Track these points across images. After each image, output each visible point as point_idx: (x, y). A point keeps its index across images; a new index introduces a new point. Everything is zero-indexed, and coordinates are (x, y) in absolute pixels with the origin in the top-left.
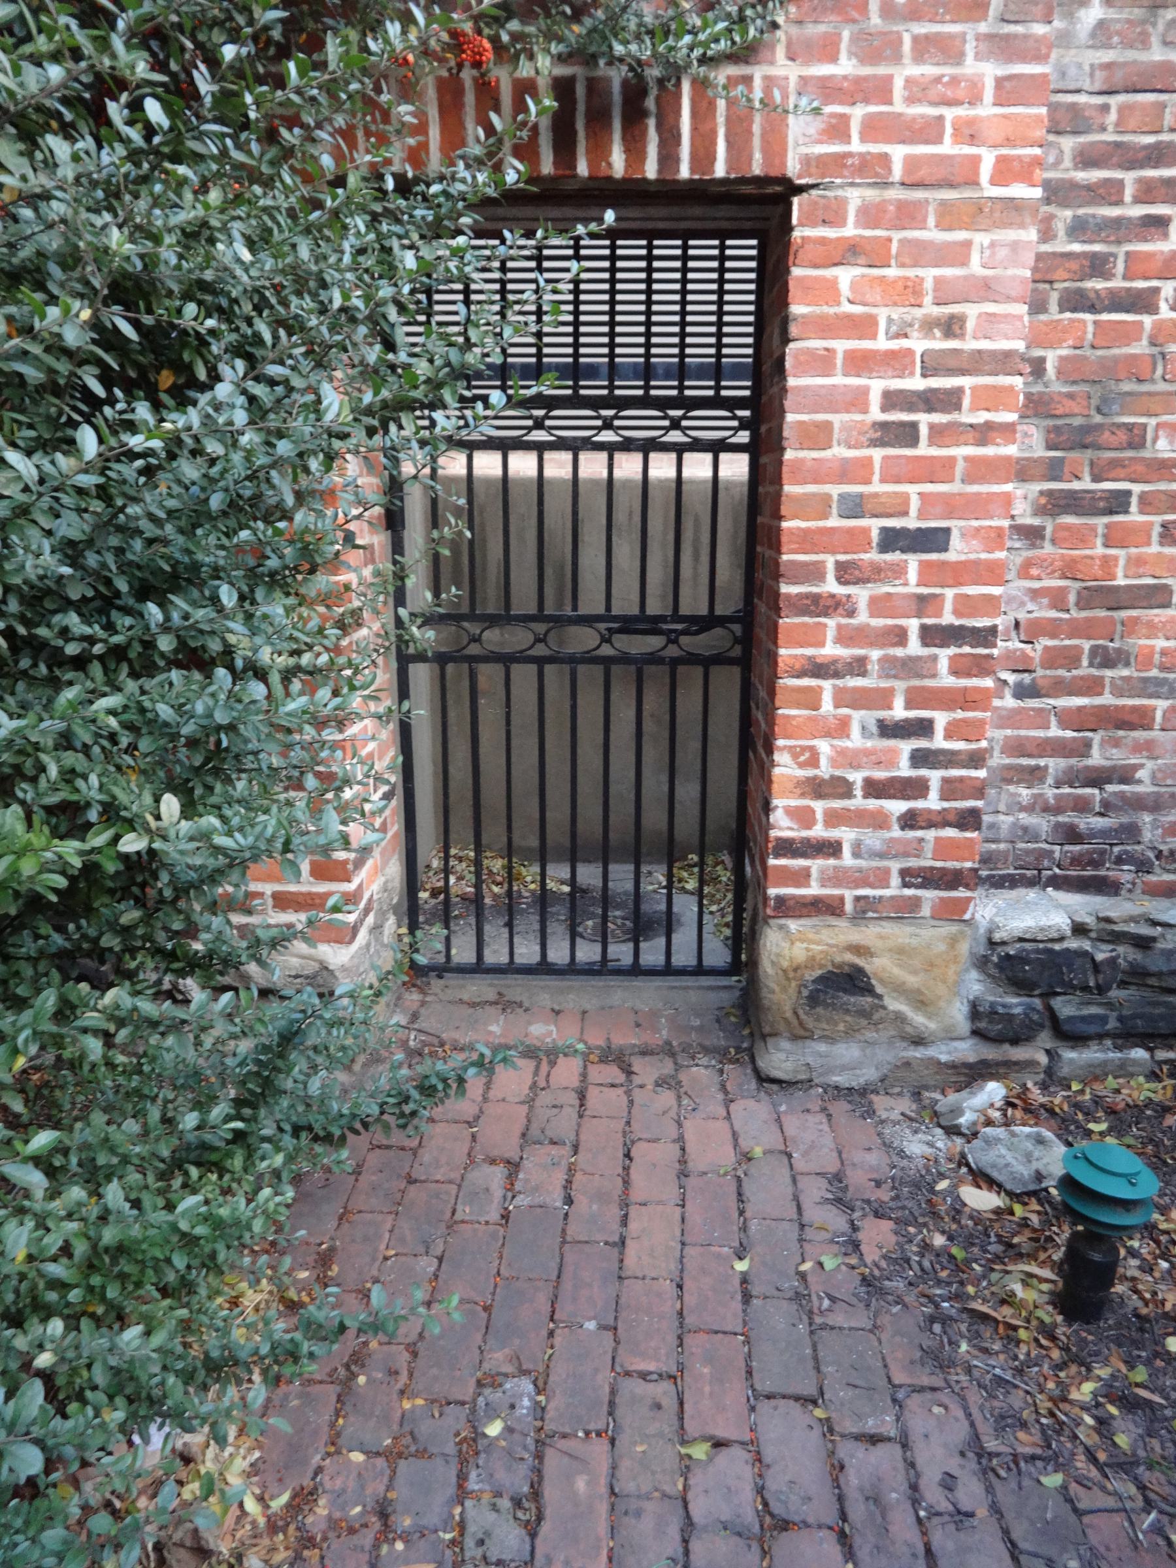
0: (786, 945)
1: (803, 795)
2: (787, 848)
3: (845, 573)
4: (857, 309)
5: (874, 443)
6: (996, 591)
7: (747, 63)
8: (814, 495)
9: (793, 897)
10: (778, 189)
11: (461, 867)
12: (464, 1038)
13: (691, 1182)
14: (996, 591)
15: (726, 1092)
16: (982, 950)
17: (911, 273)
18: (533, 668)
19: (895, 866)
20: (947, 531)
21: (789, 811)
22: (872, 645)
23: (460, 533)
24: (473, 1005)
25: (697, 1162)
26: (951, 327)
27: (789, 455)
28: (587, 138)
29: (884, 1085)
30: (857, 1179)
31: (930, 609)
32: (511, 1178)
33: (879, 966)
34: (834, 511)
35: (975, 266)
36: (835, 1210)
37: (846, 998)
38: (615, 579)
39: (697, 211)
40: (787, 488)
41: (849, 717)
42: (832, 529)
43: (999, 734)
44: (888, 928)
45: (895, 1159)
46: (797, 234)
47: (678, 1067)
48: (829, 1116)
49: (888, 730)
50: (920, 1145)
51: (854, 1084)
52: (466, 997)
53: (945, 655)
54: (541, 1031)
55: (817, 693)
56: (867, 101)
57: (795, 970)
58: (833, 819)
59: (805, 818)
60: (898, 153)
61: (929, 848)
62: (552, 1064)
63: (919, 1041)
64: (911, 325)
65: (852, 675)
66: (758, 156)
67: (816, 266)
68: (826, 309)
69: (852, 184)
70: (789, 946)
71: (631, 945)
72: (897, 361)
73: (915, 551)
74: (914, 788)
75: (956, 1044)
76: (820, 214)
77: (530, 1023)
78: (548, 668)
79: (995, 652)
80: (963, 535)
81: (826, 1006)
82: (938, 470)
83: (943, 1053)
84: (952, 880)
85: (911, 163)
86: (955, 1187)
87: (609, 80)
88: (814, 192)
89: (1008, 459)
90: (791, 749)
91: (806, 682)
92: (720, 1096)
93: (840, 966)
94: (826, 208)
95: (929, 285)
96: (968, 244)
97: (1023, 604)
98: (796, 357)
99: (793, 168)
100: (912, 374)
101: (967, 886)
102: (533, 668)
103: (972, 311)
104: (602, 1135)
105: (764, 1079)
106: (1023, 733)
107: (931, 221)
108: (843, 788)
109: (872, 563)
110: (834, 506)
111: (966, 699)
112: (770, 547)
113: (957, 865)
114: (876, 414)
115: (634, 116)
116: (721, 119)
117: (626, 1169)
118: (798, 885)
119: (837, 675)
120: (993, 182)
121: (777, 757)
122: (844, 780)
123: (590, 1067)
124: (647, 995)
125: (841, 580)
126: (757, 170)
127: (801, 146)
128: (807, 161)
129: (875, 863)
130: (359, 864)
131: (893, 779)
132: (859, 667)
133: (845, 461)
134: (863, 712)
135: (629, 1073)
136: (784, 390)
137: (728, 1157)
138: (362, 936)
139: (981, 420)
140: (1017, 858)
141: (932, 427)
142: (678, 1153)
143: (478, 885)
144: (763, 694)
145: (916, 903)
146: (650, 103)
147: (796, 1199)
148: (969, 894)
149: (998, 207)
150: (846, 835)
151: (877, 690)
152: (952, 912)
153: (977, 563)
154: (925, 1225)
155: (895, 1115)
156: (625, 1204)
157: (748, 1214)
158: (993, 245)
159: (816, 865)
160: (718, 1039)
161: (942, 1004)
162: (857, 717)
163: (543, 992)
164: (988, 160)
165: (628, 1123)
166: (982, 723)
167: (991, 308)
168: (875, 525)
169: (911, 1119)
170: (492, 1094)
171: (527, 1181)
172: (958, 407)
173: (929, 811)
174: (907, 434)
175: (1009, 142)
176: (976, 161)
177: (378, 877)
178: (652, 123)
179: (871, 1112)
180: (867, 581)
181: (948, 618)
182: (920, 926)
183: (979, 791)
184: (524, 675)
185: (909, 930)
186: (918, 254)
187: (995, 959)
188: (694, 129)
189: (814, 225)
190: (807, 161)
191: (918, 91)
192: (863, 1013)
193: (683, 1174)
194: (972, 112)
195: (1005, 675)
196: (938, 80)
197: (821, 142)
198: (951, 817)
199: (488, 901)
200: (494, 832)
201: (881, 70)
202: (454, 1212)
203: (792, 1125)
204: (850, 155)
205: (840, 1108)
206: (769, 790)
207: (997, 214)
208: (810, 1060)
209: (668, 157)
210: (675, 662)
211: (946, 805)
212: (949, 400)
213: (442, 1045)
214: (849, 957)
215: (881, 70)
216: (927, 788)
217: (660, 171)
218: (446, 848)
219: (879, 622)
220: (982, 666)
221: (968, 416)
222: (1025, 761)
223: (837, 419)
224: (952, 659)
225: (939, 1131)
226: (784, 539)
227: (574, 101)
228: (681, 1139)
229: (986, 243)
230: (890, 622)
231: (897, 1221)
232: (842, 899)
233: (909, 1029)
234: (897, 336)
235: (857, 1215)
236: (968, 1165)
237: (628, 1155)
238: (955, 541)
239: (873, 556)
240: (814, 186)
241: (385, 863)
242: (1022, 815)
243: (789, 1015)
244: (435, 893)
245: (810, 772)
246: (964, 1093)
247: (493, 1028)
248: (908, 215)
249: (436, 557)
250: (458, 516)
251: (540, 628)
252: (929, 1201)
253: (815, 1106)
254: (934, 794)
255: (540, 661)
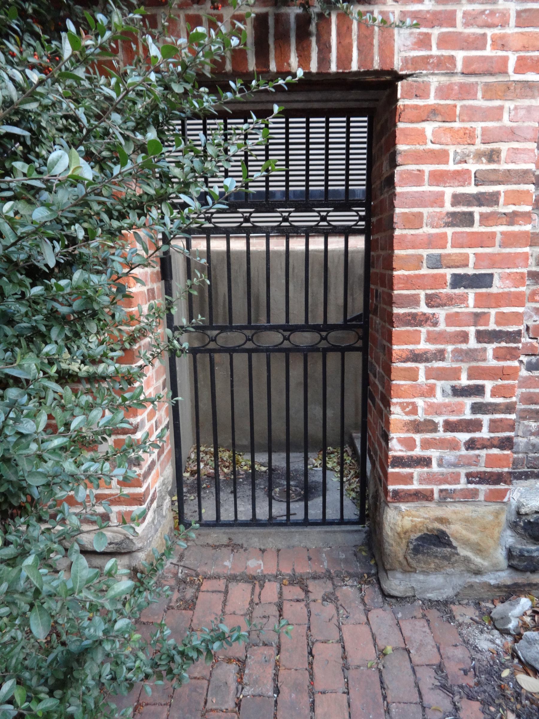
0: (399, 518)
1: (408, 431)
2: (399, 462)
3: (431, 301)
4: (437, 147)
5: (447, 225)
6: (520, 310)
7: (370, 4)
8: (413, 255)
9: (403, 490)
10: (388, 78)
11: (206, 458)
12: (212, 570)
13: (351, 674)
14: (520, 310)
15: (365, 604)
16: (513, 518)
17: (468, 125)
18: (246, 355)
19: (463, 471)
20: (491, 275)
21: (400, 440)
22: (448, 342)
23: (203, 282)
24: (215, 547)
25: (354, 659)
26: (492, 156)
27: (397, 232)
28: (276, 49)
29: (457, 599)
30: (453, 668)
31: (482, 321)
32: (241, 672)
33: (454, 530)
34: (425, 265)
35: (506, 121)
36: (443, 695)
37: (435, 549)
38: (286, 304)
39: (338, 95)
40: (397, 252)
41: (435, 385)
42: (424, 275)
43: (519, 391)
44: (459, 507)
45: (473, 653)
46: (400, 103)
47: (335, 586)
48: (428, 621)
49: (458, 392)
50: (487, 642)
51: (440, 598)
52: (210, 542)
53: (490, 348)
54: (255, 565)
55: (416, 371)
56: (441, 25)
57: (405, 533)
58: (426, 444)
59: (409, 444)
60: (460, 55)
61: (483, 461)
62: (262, 587)
63: (478, 572)
64: (468, 156)
65: (436, 360)
66: (377, 58)
67: (412, 122)
68: (418, 147)
69: (433, 74)
70: (401, 520)
71: (302, 504)
72: (460, 177)
73: (472, 287)
74: (473, 426)
75: (500, 573)
76: (414, 92)
77: (248, 559)
78: (254, 355)
79: (520, 345)
80: (500, 278)
81: (424, 554)
82: (485, 240)
83: (492, 579)
84: (498, 479)
85: (467, 61)
86: (513, 674)
87: (288, 15)
88: (410, 79)
89: (526, 233)
90: (401, 404)
91: (409, 365)
92: (361, 607)
93: (431, 530)
94: (418, 88)
95: (479, 132)
96: (501, 108)
97: (531, 316)
98: (401, 175)
99: (397, 65)
100: (470, 184)
101: (505, 482)
102: (246, 355)
103: (504, 147)
104: (293, 637)
105: (386, 595)
106: (532, 390)
107: (480, 95)
108: (432, 427)
109: (447, 295)
110: (425, 262)
111: (503, 373)
112: (383, 285)
113: (499, 470)
114: (448, 208)
115: (303, 36)
116: (355, 37)
117: (311, 664)
118: (406, 484)
119: (427, 360)
120: (516, 72)
121: (392, 409)
122: (433, 422)
123: (284, 587)
124: (313, 537)
125: (428, 305)
126: (376, 66)
127: (402, 50)
128: (406, 60)
129: (452, 470)
130: (146, 475)
131: (461, 420)
132: (440, 355)
133: (430, 235)
134: (443, 382)
135: (307, 592)
136: (394, 194)
137: (371, 654)
138: (150, 516)
139: (511, 211)
140: (529, 462)
141: (481, 215)
142: (341, 650)
143: (216, 468)
144: (379, 369)
145: (475, 493)
146: (313, 28)
147: (417, 685)
148: (506, 487)
149: (519, 86)
150: (434, 454)
151: (451, 369)
152: (497, 497)
153: (509, 294)
154: (500, 705)
155: (467, 620)
156: (312, 693)
157: (389, 699)
158: (516, 108)
159: (416, 471)
160: (357, 568)
161: (491, 551)
162: (439, 384)
163: (253, 538)
164: (512, 59)
165: (309, 628)
166: (513, 386)
167: (515, 145)
168: (448, 273)
169: (477, 622)
170: (229, 609)
171: (250, 675)
172: (497, 203)
173: (483, 439)
174: (467, 219)
175: (525, 48)
176: (505, 59)
177: (158, 478)
178: (314, 40)
179: (452, 618)
180: (445, 305)
181: (492, 326)
182: (477, 506)
183: (512, 427)
184: (240, 359)
185: (471, 508)
186: (472, 114)
187: (522, 524)
188: (339, 43)
189: (410, 98)
190: (406, 60)
191: (471, 19)
192: (445, 558)
193: (345, 668)
194: (503, 31)
195: (522, 358)
196: (483, 12)
197: (414, 49)
198: (496, 442)
199: (221, 477)
200: (224, 437)
201: (449, 7)
202: (206, 703)
203: (406, 626)
204: (431, 56)
205: (433, 614)
206: (388, 429)
207: (518, 91)
208: (414, 585)
209: (324, 60)
210: (325, 351)
211: (492, 435)
212: (491, 199)
213: (197, 575)
214: (437, 525)
215: (449, 7)
216: (482, 426)
217: (319, 68)
218: (198, 447)
219: (452, 329)
220: (512, 354)
221: (502, 209)
222: (533, 407)
223: (425, 211)
224: (495, 350)
225: (496, 632)
226: (395, 282)
227: (267, 28)
228: (341, 640)
229: (512, 107)
230: (458, 329)
231: (483, 702)
232: (432, 491)
233: (472, 566)
234: (460, 162)
235: (457, 698)
236: (518, 657)
237: (310, 653)
238: (496, 281)
239: (448, 290)
240: (411, 75)
241: (163, 469)
242: (532, 438)
243: (401, 559)
244: (192, 473)
245: (412, 418)
246: (507, 604)
247: (227, 563)
248: (466, 92)
249: (190, 295)
250: (202, 272)
251: (249, 333)
252: (500, 686)
253: (418, 613)
254: (485, 429)
255: (250, 351)
